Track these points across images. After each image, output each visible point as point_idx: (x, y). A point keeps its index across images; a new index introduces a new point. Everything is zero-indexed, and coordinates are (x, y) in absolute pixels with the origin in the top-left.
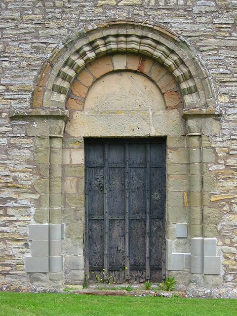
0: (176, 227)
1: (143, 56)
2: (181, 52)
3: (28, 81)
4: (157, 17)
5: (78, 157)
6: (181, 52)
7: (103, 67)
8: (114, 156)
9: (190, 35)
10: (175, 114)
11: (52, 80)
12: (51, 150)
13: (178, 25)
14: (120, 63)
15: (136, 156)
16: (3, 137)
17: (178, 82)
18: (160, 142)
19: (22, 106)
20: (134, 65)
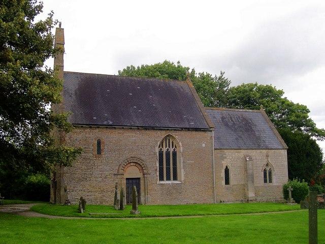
0: (142, 194)
1: (136, 163)
2: (143, 162)
3: (117, 168)
4: (139, 156)
5: (125, 181)
6: (143, 162)
7: (129, 165)
8: (130, 181)
9: (185, 217)
10: (142, 174)
11: (121, 168)
12: (121, 181)
13: (143, 158)
14: (132, 164)
15: (134, 181)
16: (321, 203)
17: (142, 168)
18: (139, 179)
19: (116, 173)
20: (135, 164)
